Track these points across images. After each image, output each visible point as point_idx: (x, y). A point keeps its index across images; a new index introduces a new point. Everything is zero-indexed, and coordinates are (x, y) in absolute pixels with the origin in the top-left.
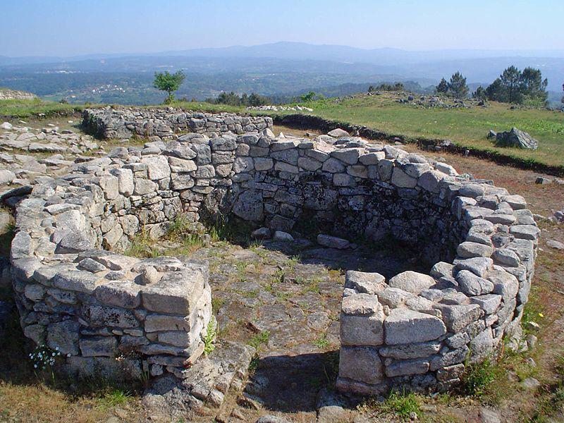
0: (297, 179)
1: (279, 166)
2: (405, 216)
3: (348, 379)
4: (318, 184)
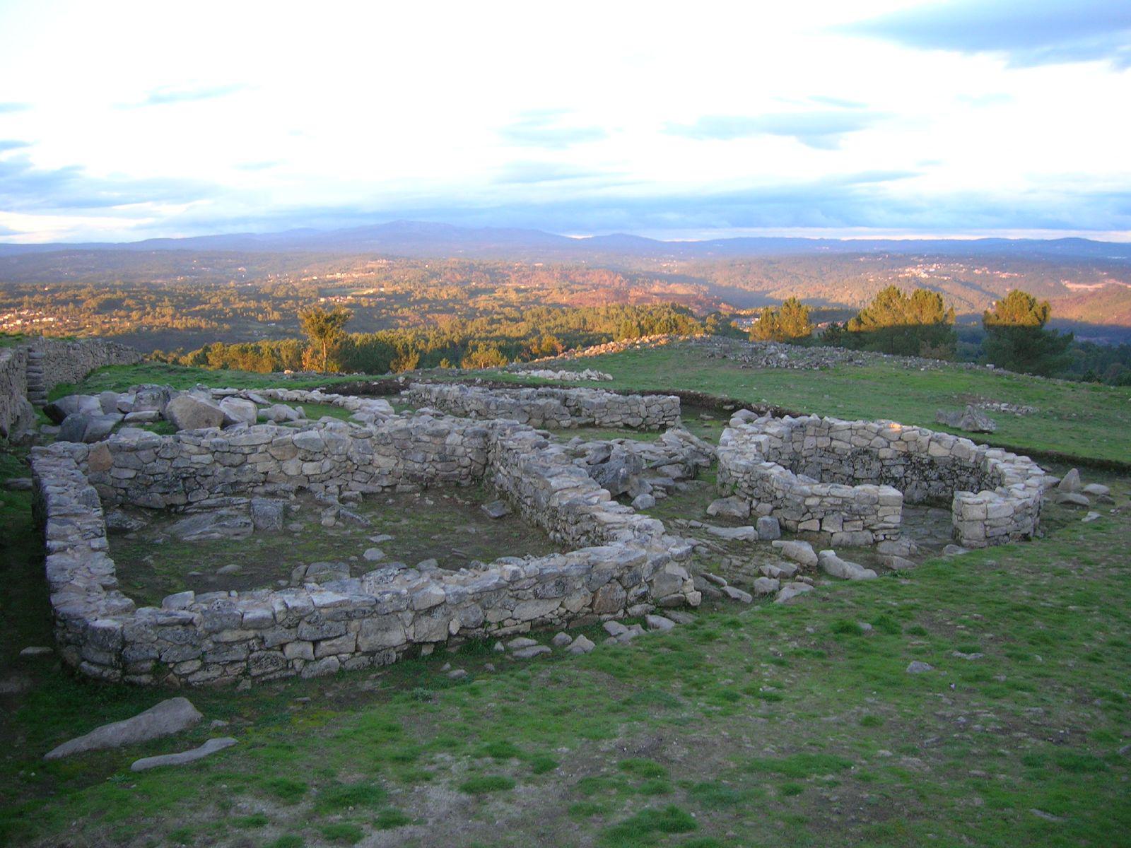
0: (849, 454)
1: (835, 443)
2: (940, 478)
3: (969, 539)
4: (866, 458)
